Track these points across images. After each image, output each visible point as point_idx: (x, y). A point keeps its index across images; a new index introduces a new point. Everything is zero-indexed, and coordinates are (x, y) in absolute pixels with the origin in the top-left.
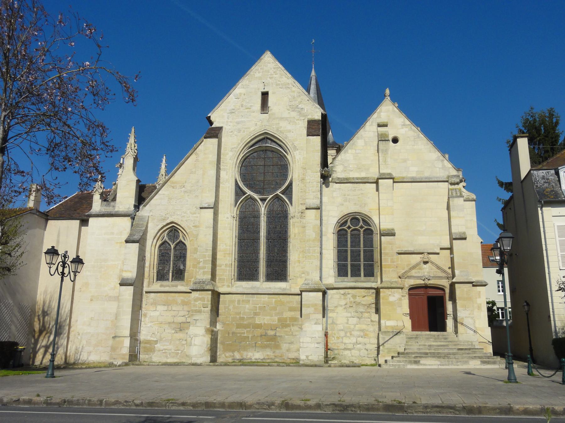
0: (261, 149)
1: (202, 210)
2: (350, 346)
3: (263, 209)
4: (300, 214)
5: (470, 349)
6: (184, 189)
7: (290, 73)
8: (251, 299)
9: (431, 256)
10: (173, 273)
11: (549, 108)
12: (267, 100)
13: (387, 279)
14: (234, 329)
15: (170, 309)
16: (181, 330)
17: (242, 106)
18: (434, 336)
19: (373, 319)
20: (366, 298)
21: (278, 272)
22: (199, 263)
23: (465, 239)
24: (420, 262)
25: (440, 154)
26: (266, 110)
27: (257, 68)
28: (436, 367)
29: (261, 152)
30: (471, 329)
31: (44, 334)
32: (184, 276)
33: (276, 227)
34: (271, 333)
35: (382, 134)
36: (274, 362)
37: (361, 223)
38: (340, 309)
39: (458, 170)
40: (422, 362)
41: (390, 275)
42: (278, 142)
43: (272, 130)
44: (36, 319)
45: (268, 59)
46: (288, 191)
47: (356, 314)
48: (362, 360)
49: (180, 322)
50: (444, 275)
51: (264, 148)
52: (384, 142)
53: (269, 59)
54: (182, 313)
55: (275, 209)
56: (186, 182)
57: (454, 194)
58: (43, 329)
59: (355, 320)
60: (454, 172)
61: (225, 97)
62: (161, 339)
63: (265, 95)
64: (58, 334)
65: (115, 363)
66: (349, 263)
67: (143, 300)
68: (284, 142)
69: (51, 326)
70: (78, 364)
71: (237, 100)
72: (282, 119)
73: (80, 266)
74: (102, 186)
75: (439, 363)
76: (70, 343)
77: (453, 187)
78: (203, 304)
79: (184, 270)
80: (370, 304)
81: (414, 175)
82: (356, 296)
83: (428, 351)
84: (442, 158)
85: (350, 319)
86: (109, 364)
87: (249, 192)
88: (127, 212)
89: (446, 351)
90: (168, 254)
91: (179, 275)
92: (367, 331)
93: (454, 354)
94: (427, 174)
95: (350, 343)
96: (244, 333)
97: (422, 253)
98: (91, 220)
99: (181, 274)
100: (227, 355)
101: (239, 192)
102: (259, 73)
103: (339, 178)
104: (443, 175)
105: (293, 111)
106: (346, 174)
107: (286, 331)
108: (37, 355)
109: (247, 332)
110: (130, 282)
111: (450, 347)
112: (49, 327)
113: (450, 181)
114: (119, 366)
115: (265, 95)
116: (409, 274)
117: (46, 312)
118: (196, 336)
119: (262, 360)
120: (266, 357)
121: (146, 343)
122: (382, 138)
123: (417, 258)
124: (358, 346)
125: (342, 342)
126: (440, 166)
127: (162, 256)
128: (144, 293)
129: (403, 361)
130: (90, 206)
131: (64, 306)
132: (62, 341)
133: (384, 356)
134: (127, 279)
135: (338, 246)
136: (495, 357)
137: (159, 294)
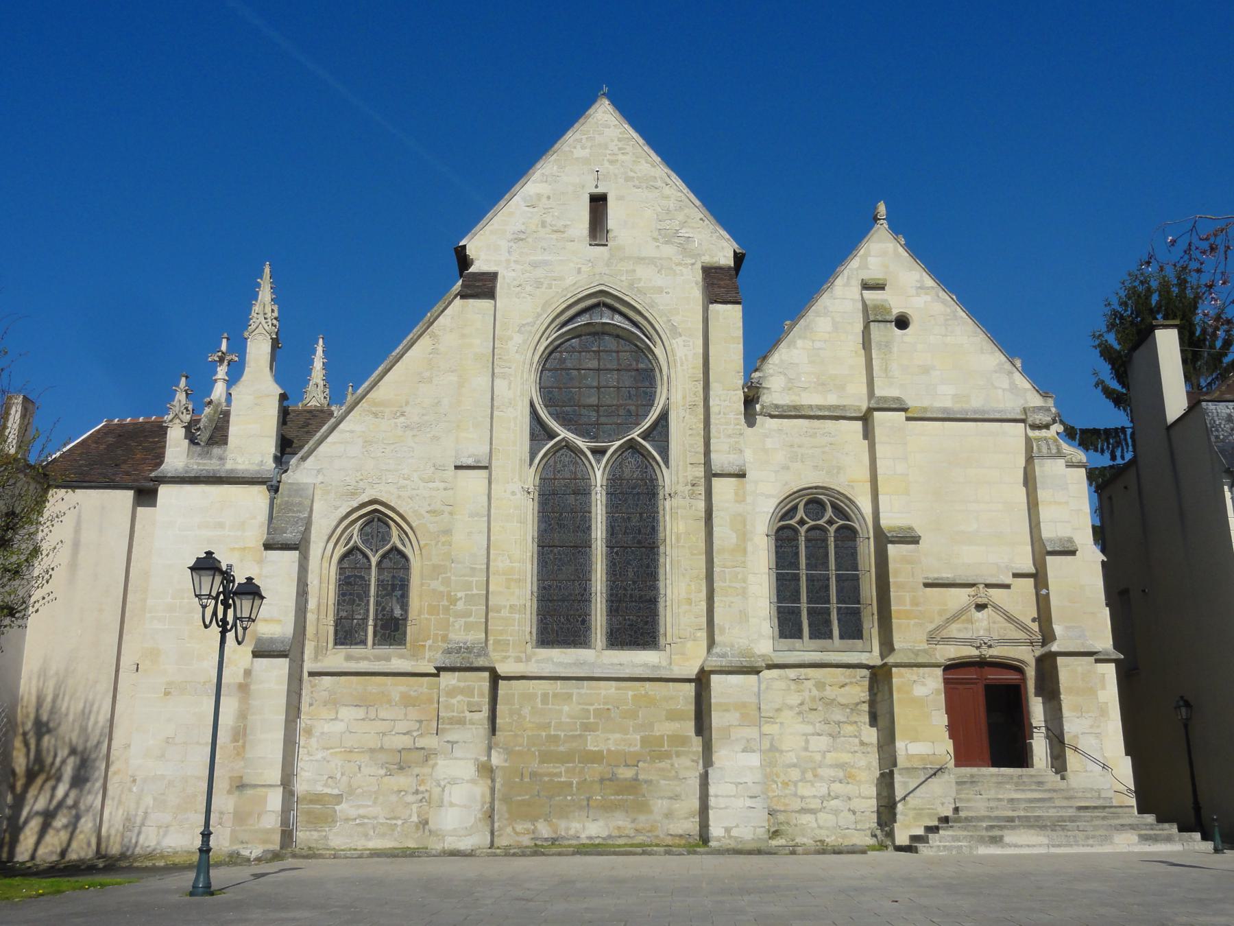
0: (592, 330)
1: (460, 472)
2: (815, 804)
3: (599, 474)
4: (690, 487)
5: (1104, 807)
6: (402, 419)
7: (658, 152)
8: (575, 691)
9: (992, 591)
10: (375, 626)
12: (599, 212)
13: (905, 645)
14: (535, 765)
15: (372, 715)
16: (401, 768)
17: (543, 224)
18: (1011, 777)
19: (866, 740)
20: (847, 688)
21: (637, 624)
22: (454, 601)
23: (1073, 553)
24: (969, 606)
25: (1003, 358)
27: (577, 135)
28: (1043, 851)
29: (591, 339)
30: (1095, 761)
31: (39, 781)
32: (405, 633)
33: (629, 518)
34: (626, 773)
35: (876, 307)
36: (657, 845)
37: (829, 512)
38: (787, 716)
39: (1045, 395)
40: (1007, 839)
41: (908, 637)
42: (631, 314)
43: (618, 286)
44: (18, 743)
47: (826, 727)
48: (844, 837)
49: (400, 747)
50: (1021, 635)
51: (599, 329)
52: (882, 325)
54: (402, 726)
55: (627, 473)
56: (407, 403)
57: (1045, 450)
58: (36, 768)
59: (821, 743)
60: (1036, 400)
61: (502, 203)
62: (351, 791)
63: (598, 202)
64: (80, 781)
65: (245, 853)
66: (804, 606)
67: (304, 693)
68: (647, 314)
69: (58, 760)
70: (135, 858)
71: (531, 209)
72: (640, 260)
73: (257, 602)
74: (190, 408)
75: (1046, 841)
76: (108, 802)
77: (1037, 433)
78: (469, 704)
79: (405, 619)
80: (857, 704)
81: (948, 403)
82: (824, 684)
83: (1010, 814)
84: (1008, 366)
85: (813, 739)
86: (231, 855)
87: (563, 433)
88: (258, 472)
89: (1052, 813)
90: (362, 578)
91: (392, 630)
93: (1072, 819)
94: (976, 403)
95: (815, 797)
96: (559, 775)
98: (164, 491)
99: (397, 629)
100: (519, 828)
101: (539, 432)
102: (583, 148)
103: (777, 406)
104: (1012, 405)
105: (667, 243)
106: (793, 398)
107: (663, 770)
108: (22, 837)
109: (567, 771)
110: (280, 647)
111: (1058, 803)
112: (53, 763)
113: (1030, 421)
114: (259, 859)
115: (598, 202)
116: (945, 634)
117: (47, 724)
118: (453, 782)
119: (604, 839)
120: (615, 833)
121: (311, 802)
122: (872, 317)
123: (961, 597)
124: (834, 803)
125: (795, 795)
126: (1006, 386)
127: (348, 584)
128: (305, 674)
129: (965, 837)
130: (159, 458)
131: (95, 708)
132: (90, 798)
133: (907, 827)
135: (778, 566)
136: (1161, 826)
137: (343, 678)
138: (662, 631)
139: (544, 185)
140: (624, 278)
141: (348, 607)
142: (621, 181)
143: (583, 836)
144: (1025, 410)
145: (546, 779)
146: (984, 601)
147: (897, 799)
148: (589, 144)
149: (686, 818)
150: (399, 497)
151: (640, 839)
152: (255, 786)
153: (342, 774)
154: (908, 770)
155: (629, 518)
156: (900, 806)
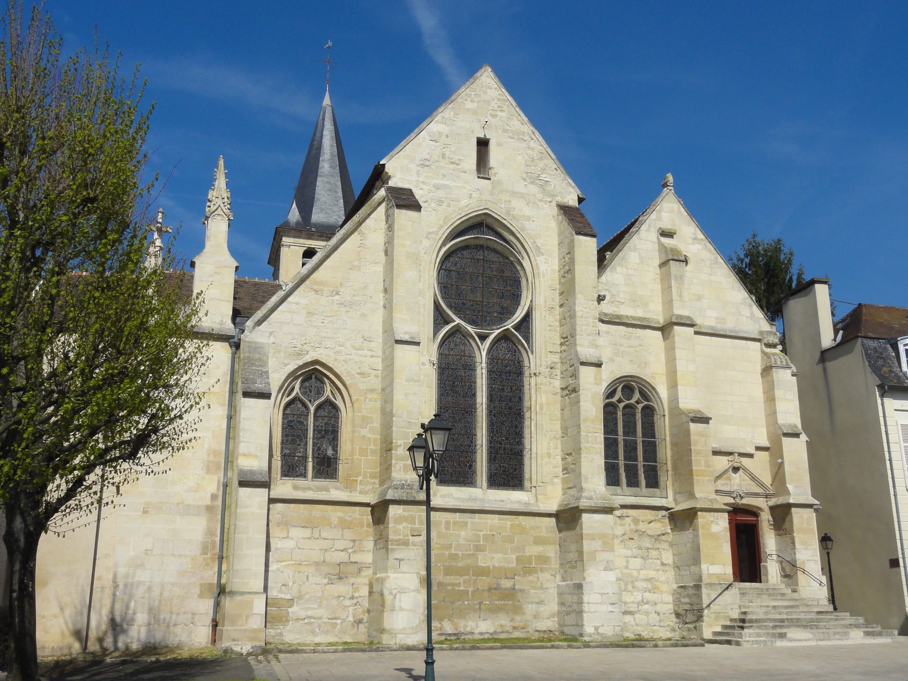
2: (633, 608)
4: (549, 369)
6: (337, 297)
8: (470, 520)
11: (776, 239)
12: (478, 153)
15: (316, 535)
16: (340, 578)
19: (665, 562)
26: (484, 173)
27: (468, 91)
28: (813, 643)
33: (503, 389)
34: (507, 584)
40: (789, 635)
41: (704, 492)
43: (499, 211)
45: (487, 78)
46: (525, 324)
47: (640, 551)
48: (653, 631)
53: (489, 80)
54: (340, 545)
56: (341, 285)
61: (413, 135)
63: (483, 144)
68: (519, 235)
71: (433, 143)
72: (514, 193)
75: (810, 636)
78: (412, 529)
79: (336, 459)
81: (712, 323)
85: (631, 560)
87: (458, 321)
91: (327, 467)
92: (657, 581)
94: (729, 325)
95: (633, 602)
97: (731, 454)
99: (329, 466)
101: (440, 318)
102: (472, 101)
105: (532, 183)
106: (615, 309)
109: (465, 582)
113: (765, 341)
115: (483, 144)
118: (403, 591)
119: (491, 634)
120: (499, 630)
124: (646, 607)
126: (748, 314)
133: (711, 626)
134: (252, 472)
137: (292, 505)
138: (527, 476)
139: (443, 126)
140: (502, 206)
141: (289, 446)
142: (500, 131)
143: (477, 632)
144: (761, 333)
145: (450, 588)
146: (739, 465)
147: (704, 606)
148: (476, 99)
149: (548, 618)
150: (336, 360)
151: (517, 634)
152: (243, 593)
153: (294, 583)
154: (711, 585)
155: (503, 389)
156: (706, 612)
